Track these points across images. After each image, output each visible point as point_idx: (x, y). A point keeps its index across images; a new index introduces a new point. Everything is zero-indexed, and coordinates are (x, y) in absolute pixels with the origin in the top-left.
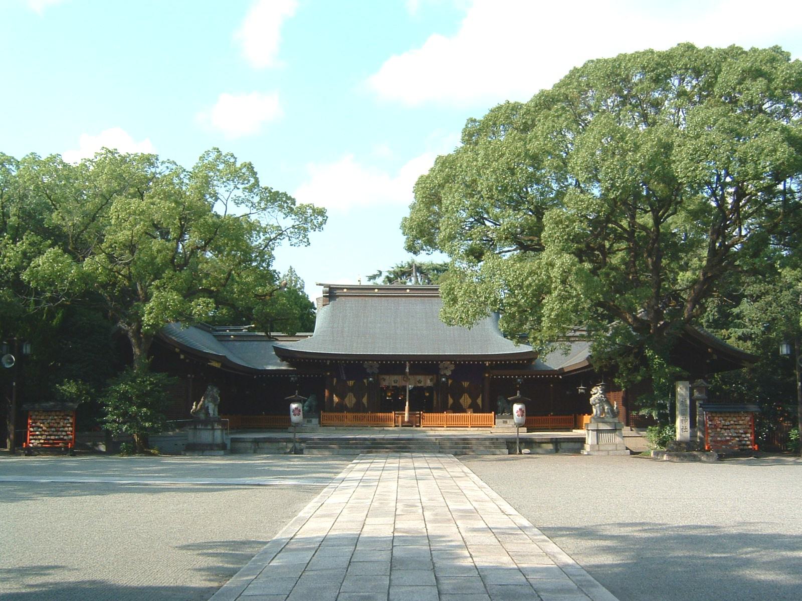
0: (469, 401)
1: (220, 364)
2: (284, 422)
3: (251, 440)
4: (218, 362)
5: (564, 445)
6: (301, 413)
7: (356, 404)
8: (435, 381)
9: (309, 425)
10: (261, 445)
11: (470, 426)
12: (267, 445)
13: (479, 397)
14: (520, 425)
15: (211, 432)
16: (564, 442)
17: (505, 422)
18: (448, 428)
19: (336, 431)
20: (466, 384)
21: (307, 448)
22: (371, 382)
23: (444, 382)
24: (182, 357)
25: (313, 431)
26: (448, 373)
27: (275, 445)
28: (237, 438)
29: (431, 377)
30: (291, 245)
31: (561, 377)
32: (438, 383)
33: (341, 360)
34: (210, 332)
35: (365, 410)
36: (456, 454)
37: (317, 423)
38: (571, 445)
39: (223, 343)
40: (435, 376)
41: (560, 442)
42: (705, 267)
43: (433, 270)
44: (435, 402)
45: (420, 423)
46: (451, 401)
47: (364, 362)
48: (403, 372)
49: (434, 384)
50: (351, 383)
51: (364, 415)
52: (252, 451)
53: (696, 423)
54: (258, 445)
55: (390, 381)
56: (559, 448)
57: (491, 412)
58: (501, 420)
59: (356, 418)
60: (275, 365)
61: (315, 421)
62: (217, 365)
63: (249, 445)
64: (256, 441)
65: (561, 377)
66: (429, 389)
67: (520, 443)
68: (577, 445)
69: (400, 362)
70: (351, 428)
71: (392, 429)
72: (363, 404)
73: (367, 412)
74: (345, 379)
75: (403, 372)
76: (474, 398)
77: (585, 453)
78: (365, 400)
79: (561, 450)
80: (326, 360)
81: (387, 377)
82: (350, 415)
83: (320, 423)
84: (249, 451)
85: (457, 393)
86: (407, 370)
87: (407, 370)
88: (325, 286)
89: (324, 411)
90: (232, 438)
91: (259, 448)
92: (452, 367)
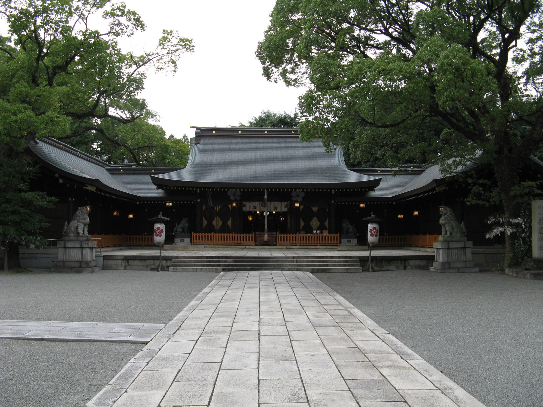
0: (318, 223)
1: (95, 188)
3: (122, 258)
4: (93, 186)
5: (412, 263)
6: (164, 234)
8: (289, 206)
9: (182, 244)
10: (131, 262)
11: (319, 244)
13: (326, 220)
15: (80, 250)
16: (411, 259)
17: (349, 241)
18: (301, 247)
19: (204, 249)
20: (315, 209)
21: (173, 265)
22: (234, 207)
23: (297, 207)
24: (61, 181)
26: (300, 199)
28: (108, 256)
29: (286, 203)
30: (129, 36)
31: (394, 203)
32: (291, 208)
33: (209, 188)
34: (104, 167)
35: (229, 232)
37: (189, 242)
38: (418, 262)
39: (114, 176)
40: (289, 202)
41: (408, 260)
42: (520, 106)
44: (289, 224)
45: (276, 242)
46: (302, 224)
47: (228, 190)
49: (288, 209)
50: (218, 208)
51: (229, 235)
52: (123, 268)
54: (128, 262)
55: (249, 206)
56: (407, 264)
57: (337, 233)
58: (346, 240)
60: (155, 192)
62: (93, 189)
63: (120, 262)
64: (127, 259)
65: (394, 203)
66: (284, 214)
67: (372, 261)
69: (260, 189)
70: (217, 246)
71: (412, 249)
72: (228, 225)
73: (232, 233)
74: (212, 205)
76: (322, 222)
77: (433, 270)
78: (230, 223)
79: (408, 267)
80: (197, 188)
81: (247, 204)
83: (191, 242)
84: (119, 268)
85: (307, 215)
86: (266, 197)
87: (266, 197)
88: (197, 128)
89: (195, 232)
90: (104, 256)
91: (128, 265)
92: (303, 195)
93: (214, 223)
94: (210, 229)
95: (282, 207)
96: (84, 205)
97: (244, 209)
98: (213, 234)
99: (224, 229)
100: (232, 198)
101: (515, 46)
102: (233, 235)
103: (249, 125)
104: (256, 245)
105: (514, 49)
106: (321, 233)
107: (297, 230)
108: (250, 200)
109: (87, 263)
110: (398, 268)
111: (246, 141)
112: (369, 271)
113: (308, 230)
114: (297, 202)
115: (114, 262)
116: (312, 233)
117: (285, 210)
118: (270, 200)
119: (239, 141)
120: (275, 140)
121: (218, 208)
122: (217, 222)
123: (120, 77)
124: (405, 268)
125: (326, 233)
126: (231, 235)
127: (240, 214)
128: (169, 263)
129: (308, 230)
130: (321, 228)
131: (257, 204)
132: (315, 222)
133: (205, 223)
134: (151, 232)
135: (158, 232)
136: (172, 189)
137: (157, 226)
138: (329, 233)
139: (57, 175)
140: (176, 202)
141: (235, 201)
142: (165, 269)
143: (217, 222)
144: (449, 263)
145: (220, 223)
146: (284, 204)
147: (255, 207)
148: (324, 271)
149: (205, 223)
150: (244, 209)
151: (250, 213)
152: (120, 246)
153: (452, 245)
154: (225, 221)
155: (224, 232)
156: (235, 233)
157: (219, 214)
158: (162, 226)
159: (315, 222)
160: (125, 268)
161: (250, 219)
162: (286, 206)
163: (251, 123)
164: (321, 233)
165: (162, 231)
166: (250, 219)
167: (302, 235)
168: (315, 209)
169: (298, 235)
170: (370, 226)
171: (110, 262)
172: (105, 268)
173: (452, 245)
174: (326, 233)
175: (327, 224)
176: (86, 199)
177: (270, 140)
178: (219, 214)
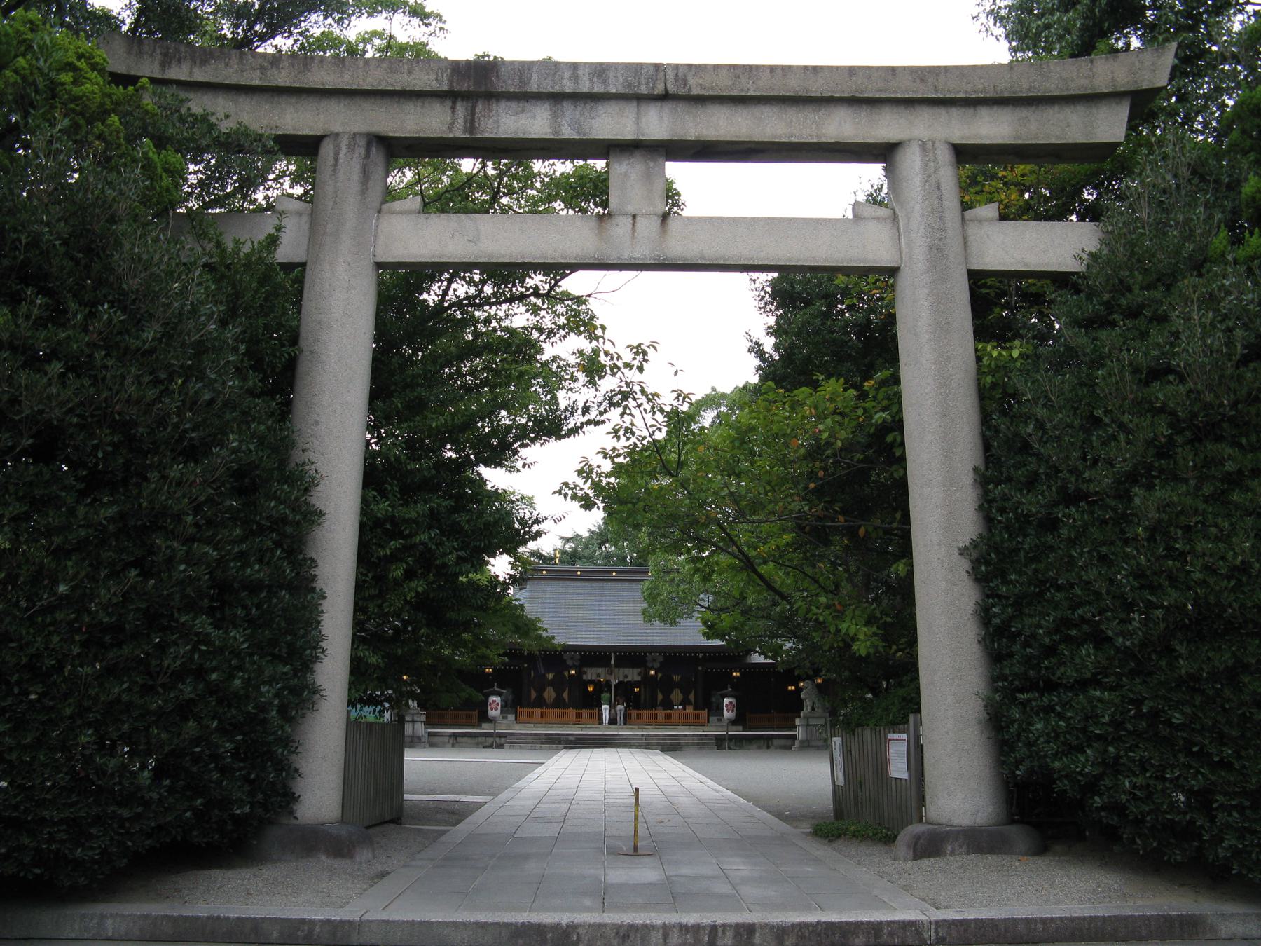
0: (681, 697)
2: (484, 717)
5: (776, 742)
7: (555, 699)
12: (465, 739)
14: (733, 722)
17: (816, 452)
25: (509, 727)
26: (657, 665)
27: (476, 740)
35: (565, 706)
36: (663, 750)
38: (782, 742)
43: (173, 532)
46: (660, 697)
48: (607, 664)
50: (550, 676)
53: (585, 159)
55: (591, 673)
59: (557, 716)
61: (511, 717)
62: (898, 768)
63: (446, 739)
64: (454, 735)
68: (789, 742)
75: (607, 664)
76: (686, 693)
78: (565, 695)
81: (588, 670)
82: (551, 711)
92: (661, 659)
93: (546, 695)
94: (540, 703)
95: (633, 675)
97: (585, 677)
99: (558, 703)
100: (570, 663)
102: (571, 710)
103: (587, 534)
106: (684, 709)
107: (653, 705)
108: (591, 665)
109: (419, 738)
110: (759, 748)
111: (587, 586)
113: (668, 705)
114: (652, 668)
115: (440, 739)
116: (672, 708)
117: (638, 678)
118: (618, 665)
119: (578, 584)
120: (627, 584)
121: (550, 676)
122: (549, 694)
124: (768, 747)
125: (690, 709)
126: (567, 711)
127: (579, 683)
128: (503, 740)
129: (668, 705)
130: (684, 703)
131: (600, 670)
132: (677, 695)
133: (533, 695)
135: (494, 705)
137: (492, 698)
138: (695, 709)
141: (574, 667)
142: (501, 746)
143: (549, 694)
144: (808, 740)
145: (554, 695)
146: (636, 671)
147: (599, 675)
148: (674, 750)
149: (533, 695)
150: (585, 677)
151: (591, 682)
153: (812, 722)
154: (559, 692)
155: (540, 707)
157: (551, 683)
158: (497, 699)
159: (677, 695)
160: (453, 746)
161: (591, 689)
162: (639, 674)
163: (592, 532)
164: (684, 709)
166: (591, 689)
167: (660, 711)
168: (676, 678)
169: (654, 711)
170: (726, 701)
171: (436, 739)
172: (432, 745)
173: (812, 722)
174: (690, 709)
175: (692, 697)
177: (620, 584)
178: (551, 683)
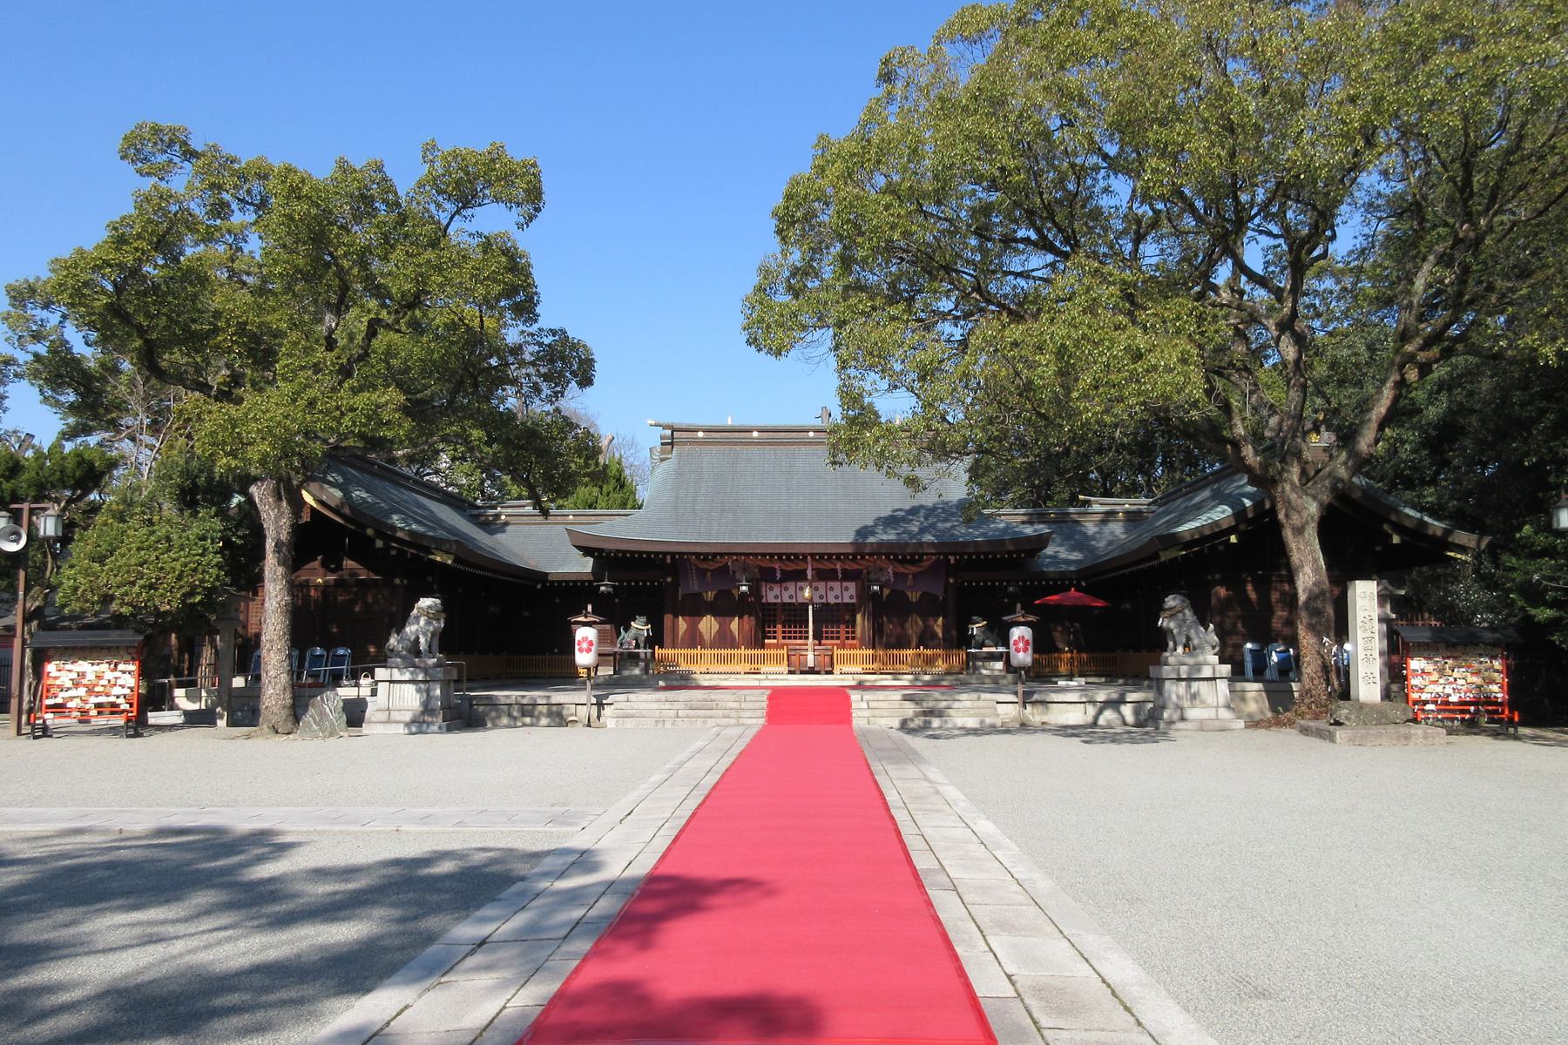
22: (743, 593)
23: (875, 593)
73: (738, 647)
89: (661, 647)
96: (1158, 609)
98: (698, 651)
101: (1324, 255)
102: (743, 651)
104: (790, 672)
105: (1322, 262)
112: (212, 723)
123: (1498, 384)
134: (568, 646)
136: (609, 559)
139: (370, 532)
140: (621, 582)
152: (498, 678)
156: (747, 647)
165: (591, 643)
176: (430, 579)
